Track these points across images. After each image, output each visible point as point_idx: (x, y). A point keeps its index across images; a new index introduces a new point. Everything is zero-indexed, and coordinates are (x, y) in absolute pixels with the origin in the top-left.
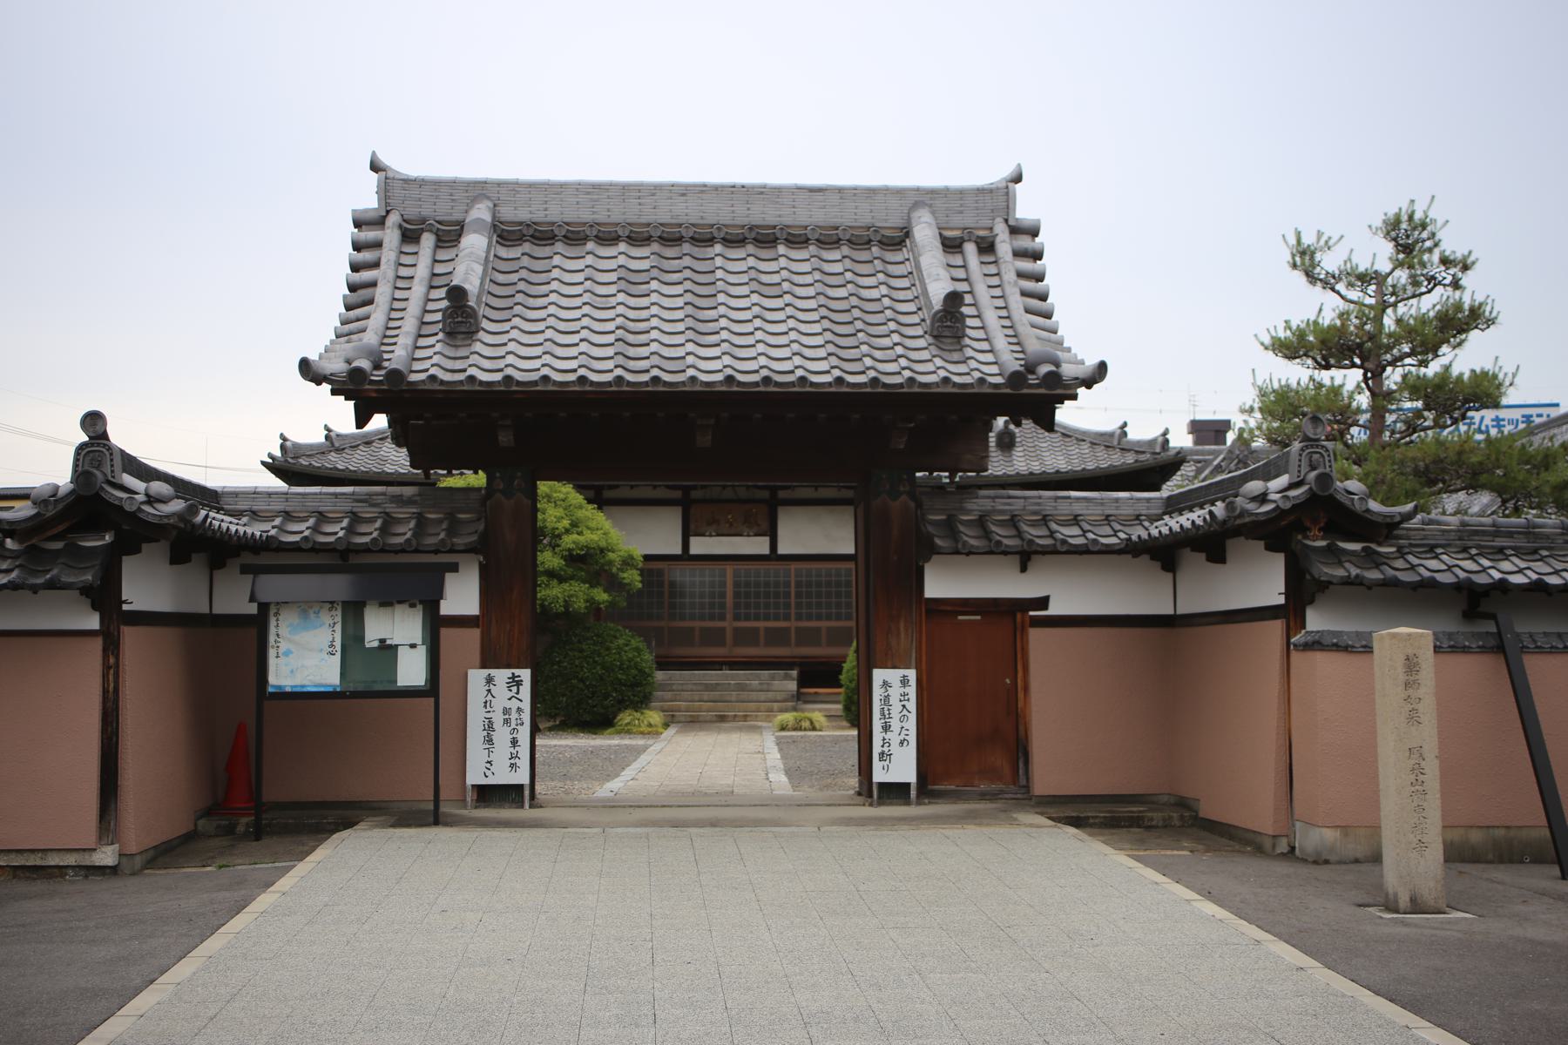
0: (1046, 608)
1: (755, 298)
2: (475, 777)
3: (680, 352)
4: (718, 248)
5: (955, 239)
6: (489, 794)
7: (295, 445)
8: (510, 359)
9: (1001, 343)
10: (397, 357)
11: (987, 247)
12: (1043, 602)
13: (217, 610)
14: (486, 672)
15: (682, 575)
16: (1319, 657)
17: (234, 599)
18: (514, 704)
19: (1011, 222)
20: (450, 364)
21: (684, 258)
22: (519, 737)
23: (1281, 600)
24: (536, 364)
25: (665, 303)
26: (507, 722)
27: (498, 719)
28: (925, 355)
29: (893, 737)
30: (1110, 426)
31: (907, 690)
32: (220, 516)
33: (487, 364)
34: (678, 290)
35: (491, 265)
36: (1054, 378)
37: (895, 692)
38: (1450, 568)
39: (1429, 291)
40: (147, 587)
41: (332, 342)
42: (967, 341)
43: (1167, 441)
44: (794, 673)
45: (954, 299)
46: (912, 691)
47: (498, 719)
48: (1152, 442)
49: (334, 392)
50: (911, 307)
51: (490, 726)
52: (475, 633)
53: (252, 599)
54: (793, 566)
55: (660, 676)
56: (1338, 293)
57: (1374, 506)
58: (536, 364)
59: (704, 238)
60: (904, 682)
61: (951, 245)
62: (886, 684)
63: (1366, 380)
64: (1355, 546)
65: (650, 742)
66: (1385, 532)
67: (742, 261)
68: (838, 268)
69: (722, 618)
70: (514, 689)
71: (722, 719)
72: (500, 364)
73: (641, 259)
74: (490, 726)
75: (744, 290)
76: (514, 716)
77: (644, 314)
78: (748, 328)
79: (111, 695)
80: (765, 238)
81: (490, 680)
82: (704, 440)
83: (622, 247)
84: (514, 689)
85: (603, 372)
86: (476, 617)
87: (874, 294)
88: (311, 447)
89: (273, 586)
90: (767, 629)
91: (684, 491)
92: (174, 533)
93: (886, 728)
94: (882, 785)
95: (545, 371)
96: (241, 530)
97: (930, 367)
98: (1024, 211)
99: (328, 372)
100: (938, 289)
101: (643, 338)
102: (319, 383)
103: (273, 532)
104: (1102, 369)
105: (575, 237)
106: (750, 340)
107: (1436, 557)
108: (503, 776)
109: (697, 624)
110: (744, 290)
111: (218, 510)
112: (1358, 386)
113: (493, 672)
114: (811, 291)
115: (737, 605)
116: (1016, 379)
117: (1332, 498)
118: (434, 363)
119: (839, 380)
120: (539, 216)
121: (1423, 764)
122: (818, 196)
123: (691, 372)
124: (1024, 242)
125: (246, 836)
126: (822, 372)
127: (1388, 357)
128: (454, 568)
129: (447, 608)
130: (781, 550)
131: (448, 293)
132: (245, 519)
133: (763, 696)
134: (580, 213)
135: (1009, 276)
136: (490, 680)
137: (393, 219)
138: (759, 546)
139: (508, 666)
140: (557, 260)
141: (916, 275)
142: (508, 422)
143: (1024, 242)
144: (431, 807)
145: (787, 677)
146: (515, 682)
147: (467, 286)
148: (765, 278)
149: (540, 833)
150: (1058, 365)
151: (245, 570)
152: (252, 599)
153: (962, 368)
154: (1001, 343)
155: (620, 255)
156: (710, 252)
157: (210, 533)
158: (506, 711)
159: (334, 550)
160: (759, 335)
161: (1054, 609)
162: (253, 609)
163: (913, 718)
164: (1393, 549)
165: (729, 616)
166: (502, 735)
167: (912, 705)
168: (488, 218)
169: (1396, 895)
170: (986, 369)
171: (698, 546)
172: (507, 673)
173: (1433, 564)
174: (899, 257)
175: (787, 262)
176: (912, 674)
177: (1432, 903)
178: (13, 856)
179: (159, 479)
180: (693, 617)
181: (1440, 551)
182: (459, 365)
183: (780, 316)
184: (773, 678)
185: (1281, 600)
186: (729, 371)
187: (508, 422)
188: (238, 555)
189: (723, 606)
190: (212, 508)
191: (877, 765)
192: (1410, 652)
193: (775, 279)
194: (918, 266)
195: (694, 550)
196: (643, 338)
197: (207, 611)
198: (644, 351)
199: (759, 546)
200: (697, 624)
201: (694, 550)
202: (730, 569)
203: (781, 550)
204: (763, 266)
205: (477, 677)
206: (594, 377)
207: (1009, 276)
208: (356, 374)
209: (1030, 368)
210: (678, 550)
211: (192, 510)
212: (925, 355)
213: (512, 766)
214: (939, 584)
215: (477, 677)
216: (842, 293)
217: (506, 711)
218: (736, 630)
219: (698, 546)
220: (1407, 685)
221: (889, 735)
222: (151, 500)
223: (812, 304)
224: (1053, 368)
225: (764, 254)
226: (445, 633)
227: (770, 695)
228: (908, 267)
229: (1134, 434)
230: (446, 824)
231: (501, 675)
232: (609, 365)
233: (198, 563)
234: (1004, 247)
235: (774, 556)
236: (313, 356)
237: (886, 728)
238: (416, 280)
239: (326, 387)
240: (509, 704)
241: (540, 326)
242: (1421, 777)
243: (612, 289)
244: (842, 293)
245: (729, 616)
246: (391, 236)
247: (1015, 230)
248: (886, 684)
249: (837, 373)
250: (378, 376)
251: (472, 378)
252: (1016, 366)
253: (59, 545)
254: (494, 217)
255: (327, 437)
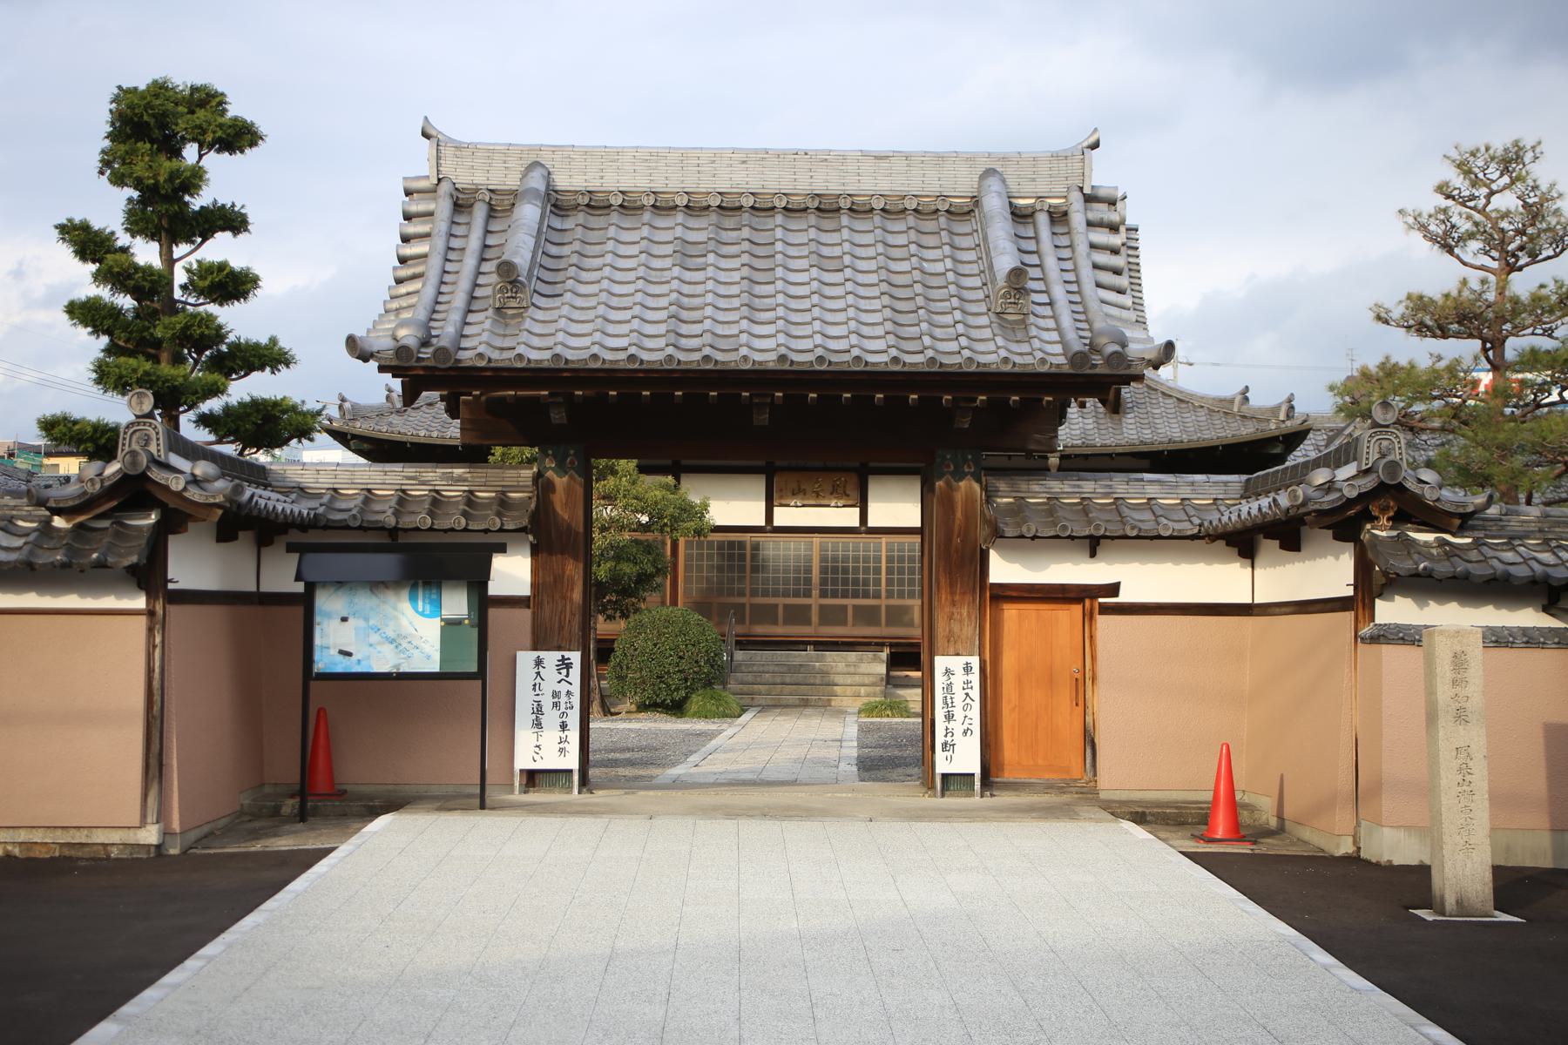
0: (1116, 595)
1: (814, 272)
2: (524, 759)
3: (734, 330)
4: (779, 219)
5: (1027, 207)
6: (532, 778)
7: (354, 406)
8: (561, 337)
9: (1066, 321)
10: (446, 331)
11: (1059, 217)
12: (1114, 589)
13: (264, 588)
14: (536, 654)
15: (776, 550)
16: (1387, 651)
17: (281, 576)
18: (564, 687)
19: (1087, 191)
20: (499, 342)
21: (740, 233)
22: (568, 721)
23: (1350, 592)
24: (586, 342)
25: (724, 274)
26: (556, 705)
27: (547, 702)
28: (987, 333)
29: (956, 726)
30: (1230, 390)
31: (970, 677)
32: (266, 494)
33: (536, 341)
34: (735, 263)
35: (545, 237)
36: (1119, 358)
37: (958, 679)
38: (1526, 561)
39: (1556, 255)
40: (193, 565)
41: (381, 316)
42: (1032, 319)
43: (1292, 407)
44: (884, 655)
45: (1017, 274)
46: (975, 678)
47: (547, 702)
48: (1275, 410)
49: (382, 369)
50: (977, 282)
51: (538, 710)
52: (526, 614)
53: (298, 578)
54: (884, 540)
55: (740, 655)
56: (1458, 257)
57: (1446, 493)
58: (586, 342)
59: (762, 209)
60: (967, 669)
61: (1020, 216)
62: (948, 672)
63: (1485, 350)
64: (1428, 537)
65: (725, 726)
66: (1457, 522)
67: (804, 232)
68: (902, 240)
69: (808, 594)
70: (564, 672)
71: (805, 704)
72: (549, 342)
73: (700, 231)
74: (538, 710)
75: (804, 264)
76: (563, 699)
77: (699, 289)
78: (806, 304)
79: (156, 708)
80: (826, 208)
81: (539, 662)
82: (762, 419)
83: (680, 217)
84: (564, 672)
85: (654, 351)
86: (528, 598)
87: (939, 267)
88: (371, 408)
89: (322, 564)
90: (855, 607)
91: (750, 471)
92: (220, 512)
93: (949, 717)
94: (945, 776)
95: (595, 349)
96: (288, 508)
97: (991, 346)
98: (1101, 177)
99: (375, 349)
100: (1005, 261)
101: (696, 315)
102: (366, 360)
103: (321, 510)
104: (1169, 347)
105: (629, 207)
106: (807, 317)
107: (1513, 549)
108: (551, 760)
109: (781, 601)
110: (804, 264)
111: (266, 486)
112: (1476, 358)
113: (542, 654)
114: (872, 265)
115: (823, 582)
116: (1077, 358)
117: (1400, 488)
118: (483, 343)
119: (895, 360)
120: (594, 185)
121: (1471, 764)
122: (884, 164)
123: (744, 351)
124: (1100, 212)
125: (290, 820)
126: (878, 351)
127: (1508, 326)
128: (502, 549)
129: (494, 589)
130: (871, 523)
131: (499, 266)
132: (293, 496)
133: (849, 680)
134: (635, 180)
135: (1082, 248)
136: (539, 662)
137: (445, 187)
138: (850, 517)
139: (559, 648)
140: (612, 232)
141: (984, 248)
142: (560, 399)
143: (1100, 212)
144: (478, 791)
145: (875, 659)
146: (565, 664)
147: (517, 260)
148: (826, 251)
149: (587, 821)
150: (1124, 346)
151: (291, 548)
152: (298, 578)
153: (1025, 348)
154: (1066, 321)
155: (674, 227)
156: (770, 223)
157: (255, 513)
158: (556, 694)
159: (383, 528)
160: (849, 286)
161: (1124, 597)
162: (300, 587)
163: (976, 706)
164: (1469, 540)
165: (815, 593)
166: (551, 717)
167: (975, 693)
168: (542, 188)
169: (1442, 897)
170: (1049, 348)
171: (785, 516)
172: (558, 655)
173: (1509, 556)
174: (966, 228)
175: (841, 238)
176: (975, 661)
177: (1479, 906)
178: (59, 832)
179: (205, 458)
180: (776, 594)
181: (1516, 542)
182: (507, 343)
183: (839, 291)
184: (861, 661)
185: (1350, 592)
186: (783, 350)
187: (560, 399)
188: (286, 532)
189: (808, 581)
190: (258, 485)
191: (940, 755)
192: (1458, 648)
193: (837, 251)
194: (985, 239)
195: (777, 522)
196: (696, 315)
197: (254, 589)
198: (697, 329)
199: (850, 517)
200: (781, 601)
201: (777, 522)
202: (817, 539)
203: (871, 523)
204: (825, 238)
205: (525, 659)
206: (646, 356)
207: (1082, 248)
208: (402, 351)
209: (1094, 348)
210: (760, 521)
211: (238, 490)
212: (987, 333)
213: (561, 750)
214: (1003, 569)
215: (525, 659)
216: (905, 266)
217: (556, 694)
218: (822, 607)
219: (785, 516)
220: (1454, 683)
221: (951, 725)
222: (195, 481)
223: (873, 278)
224: (1117, 348)
225: (827, 224)
226: (494, 613)
227: (857, 679)
228: (976, 239)
229: (1257, 400)
230: (493, 809)
231: (551, 658)
232: (661, 342)
233: (246, 539)
234: (1078, 219)
235: (864, 528)
236: (360, 333)
237: (949, 717)
238: (468, 252)
239: (373, 364)
240: (558, 687)
241: (592, 302)
242: (1468, 778)
243: (668, 263)
244: (905, 266)
245: (815, 593)
246: (443, 207)
247: (1090, 199)
248: (948, 672)
249: (894, 352)
250: (426, 353)
251: (520, 356)
252: (1077, 346)
253: (105, 524)
254: (548, 185)
255: (388, 398)
